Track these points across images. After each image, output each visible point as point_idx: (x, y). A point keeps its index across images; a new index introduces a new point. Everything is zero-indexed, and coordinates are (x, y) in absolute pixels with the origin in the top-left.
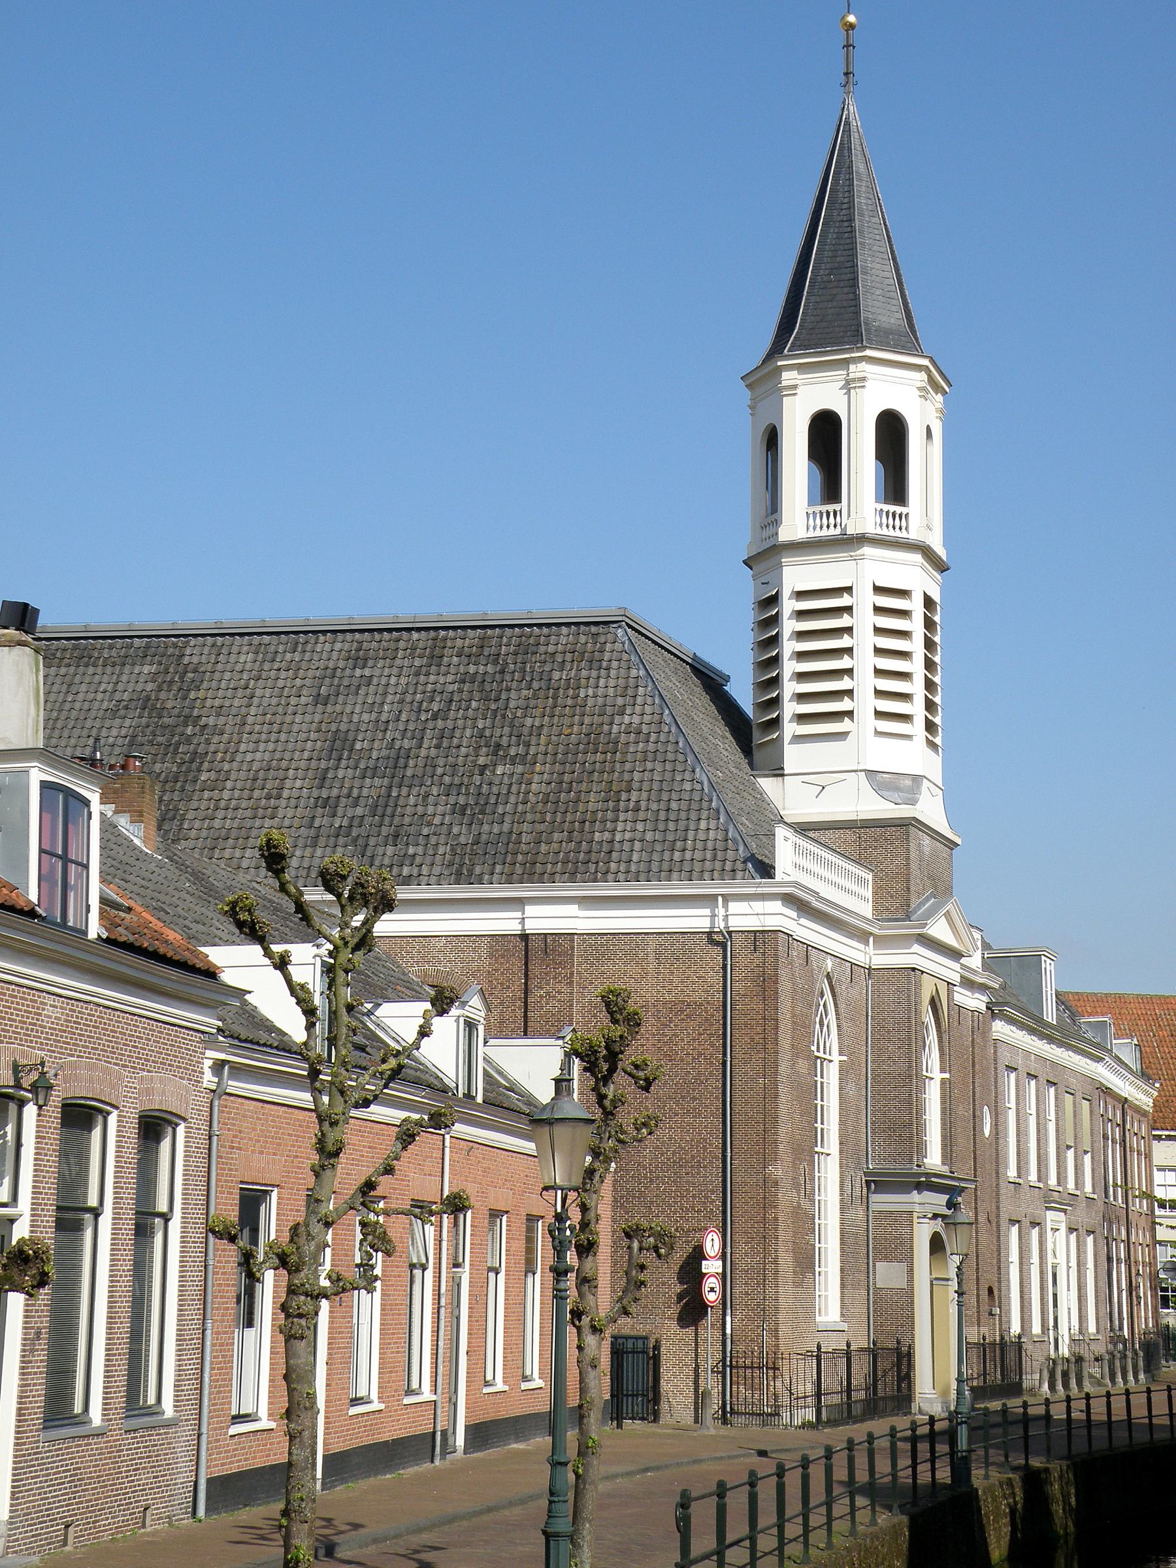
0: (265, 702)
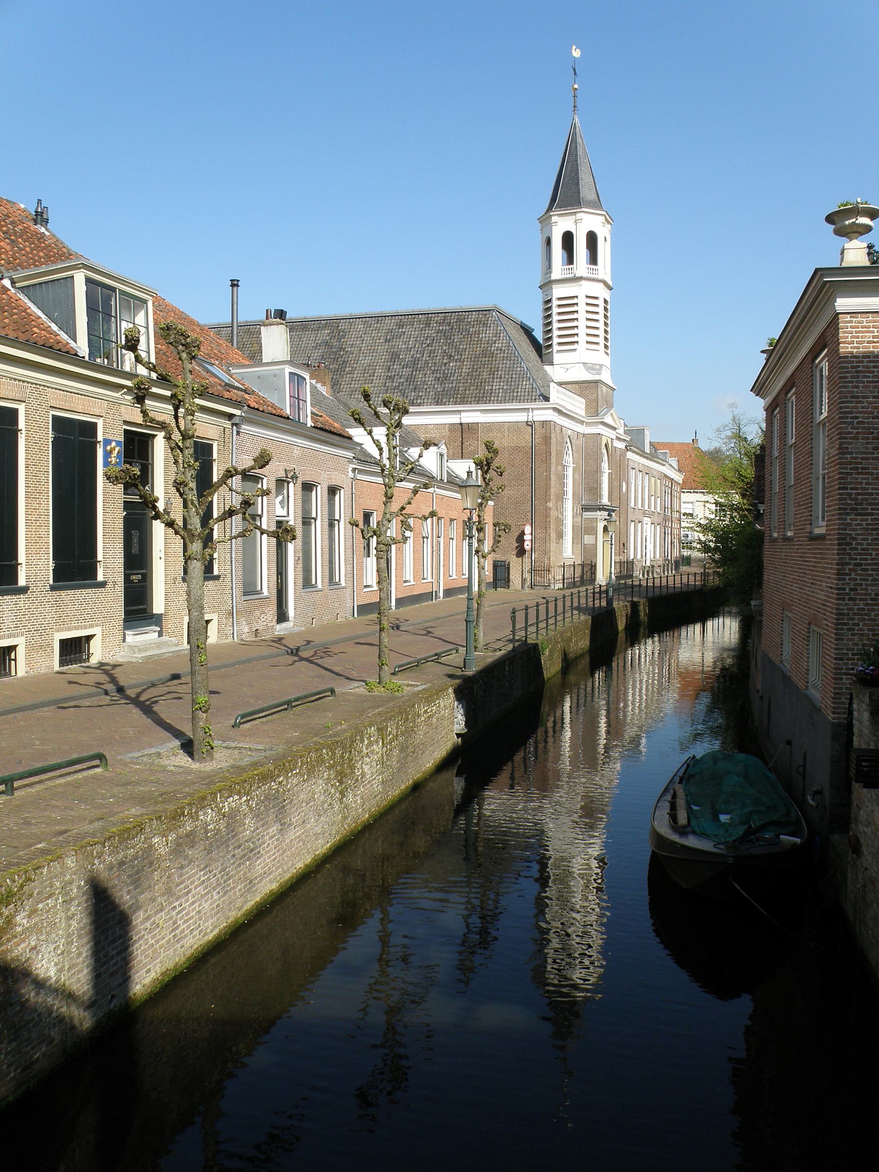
0: (368, 342)
